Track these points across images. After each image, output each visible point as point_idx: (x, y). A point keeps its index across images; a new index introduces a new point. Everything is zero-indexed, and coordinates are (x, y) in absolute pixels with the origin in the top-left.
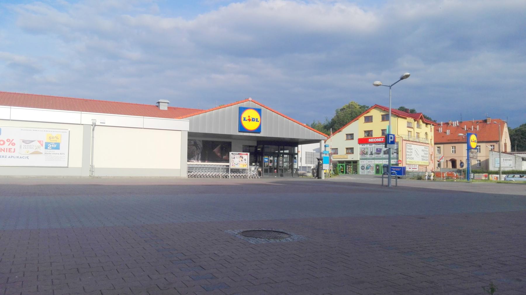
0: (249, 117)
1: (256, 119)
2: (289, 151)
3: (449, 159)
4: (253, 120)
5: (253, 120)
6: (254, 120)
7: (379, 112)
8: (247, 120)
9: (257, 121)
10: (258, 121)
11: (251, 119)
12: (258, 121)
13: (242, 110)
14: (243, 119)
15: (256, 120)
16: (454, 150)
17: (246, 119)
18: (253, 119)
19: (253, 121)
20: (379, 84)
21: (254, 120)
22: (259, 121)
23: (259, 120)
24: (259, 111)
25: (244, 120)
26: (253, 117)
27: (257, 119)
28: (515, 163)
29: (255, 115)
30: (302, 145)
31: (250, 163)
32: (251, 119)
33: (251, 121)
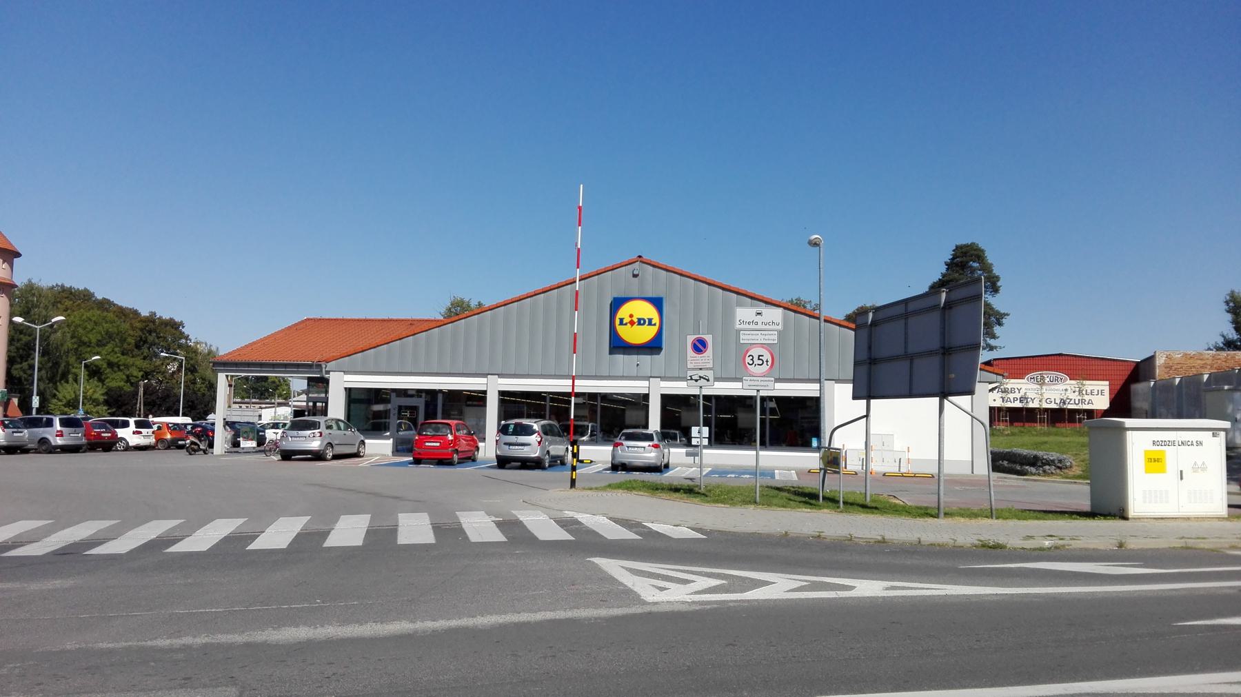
0: (631, 316)
1: (647, 321)
2: (15, 397)
3: (216, 421)
4: (641, 322)
5: (641, 322)
6: (642, 322)
7: (935, 281)
8: (626, 324)
9: (650, 324)
10: (653, 323)
11: (636, 320)
12: (653, 323)
13: (617, 303)
14: (617, 322)
15: (647, 323)
16: (760, 326)
17: (624, 322)
18: (639, 320)
19: (639, 324)
20: (802, 504)
21: (642, 322)
22: (655, 325)
23: (656, 320)
24: (657, 303)
25: (621, 323)
26: (640, 317)
27: (650, 320)
28: (1211, 682)
29: (647, 311)
30: (625, 356)
31: (450, 391)
32: (636, 320)
33: (635, 326)
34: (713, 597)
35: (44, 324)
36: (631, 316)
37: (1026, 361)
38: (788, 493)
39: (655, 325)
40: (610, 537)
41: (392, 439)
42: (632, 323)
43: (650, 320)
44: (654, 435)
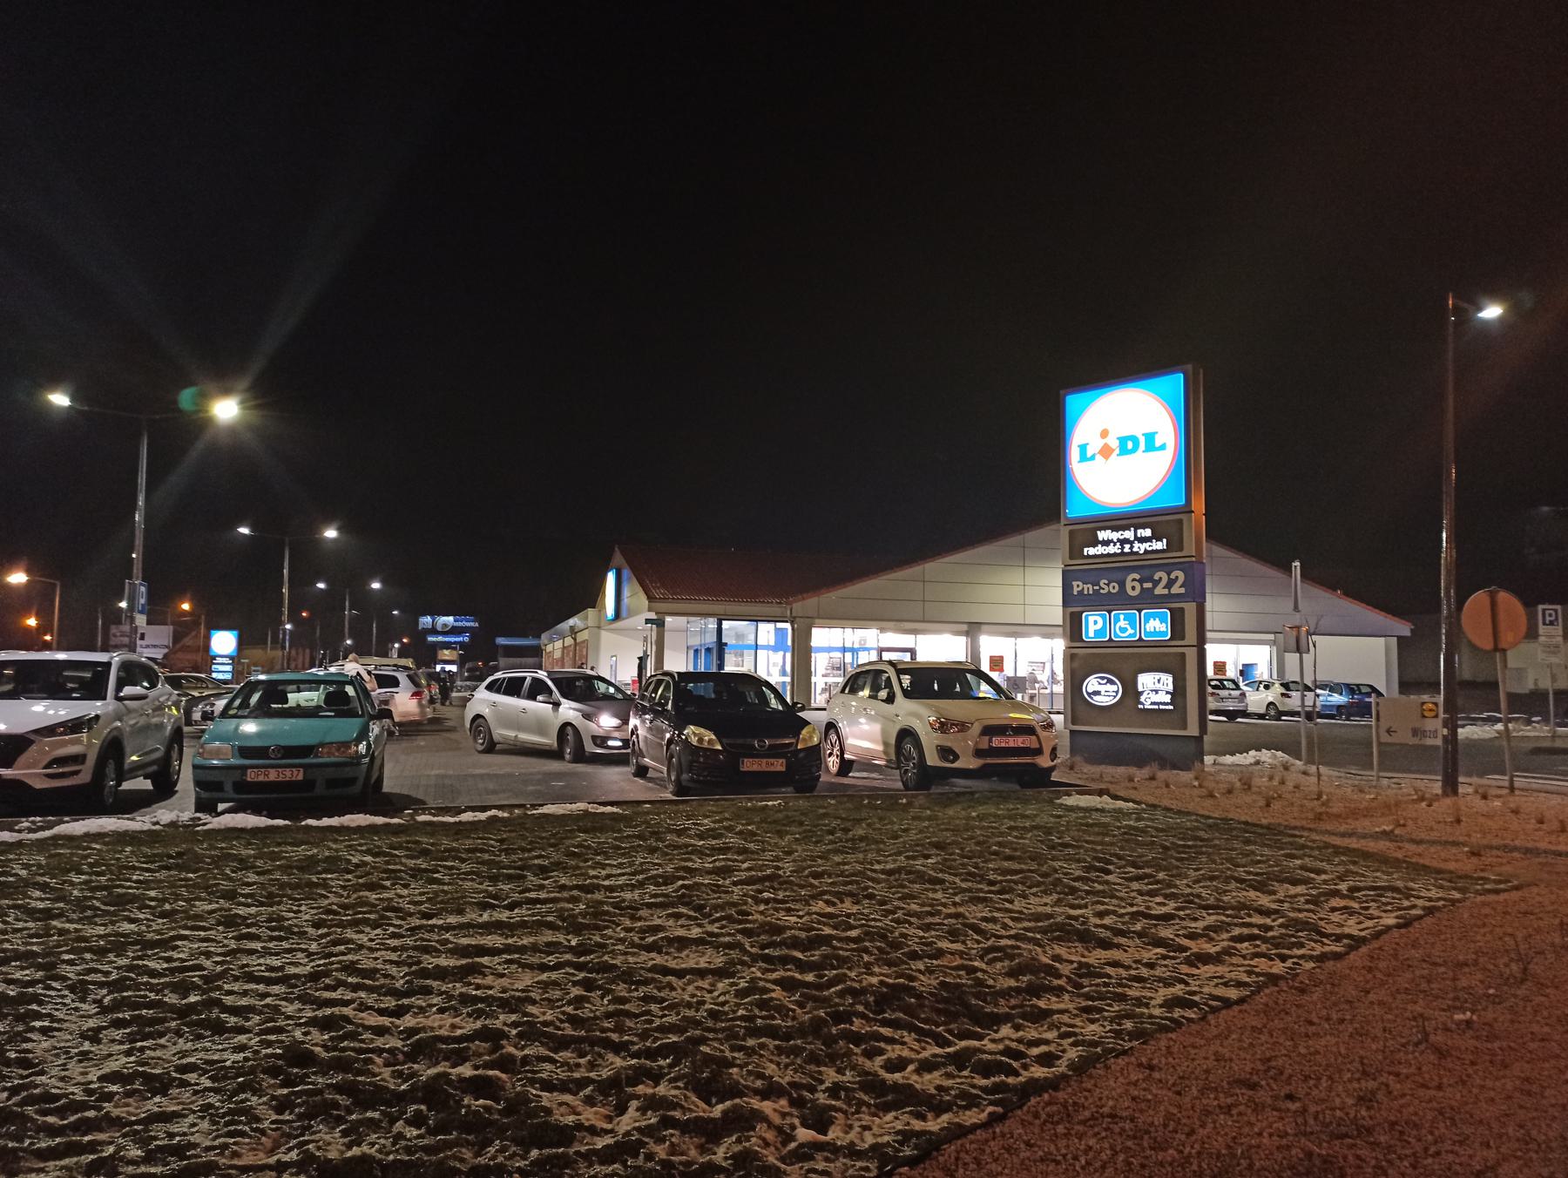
1: (1142, 441)
4: (1127, 445)
5: (1127, 445)
6: (1130, 445)
8: (1093, 458)
9: (1151, 446)
10: (1157, 445)
12: (1157, 445)
15: (1142, 446)
17: (1089, 454)
18: (1123, 440)
19: (1124, 451)
21: (1130, 445)
22: (1163, 447)
25: (1084, 458)
27: (1150, 437)
32: (1114, 443)
34: (353, 820)
35: (29, 768)
36: (1104, 434)
37: (1349, 632)
38: (1537, 849)
39: (1163, 447)
40: (38, 786)
41: (713, 696)
42: (1106, 452)
43: (1150, 437)
44: (1551, 696)
